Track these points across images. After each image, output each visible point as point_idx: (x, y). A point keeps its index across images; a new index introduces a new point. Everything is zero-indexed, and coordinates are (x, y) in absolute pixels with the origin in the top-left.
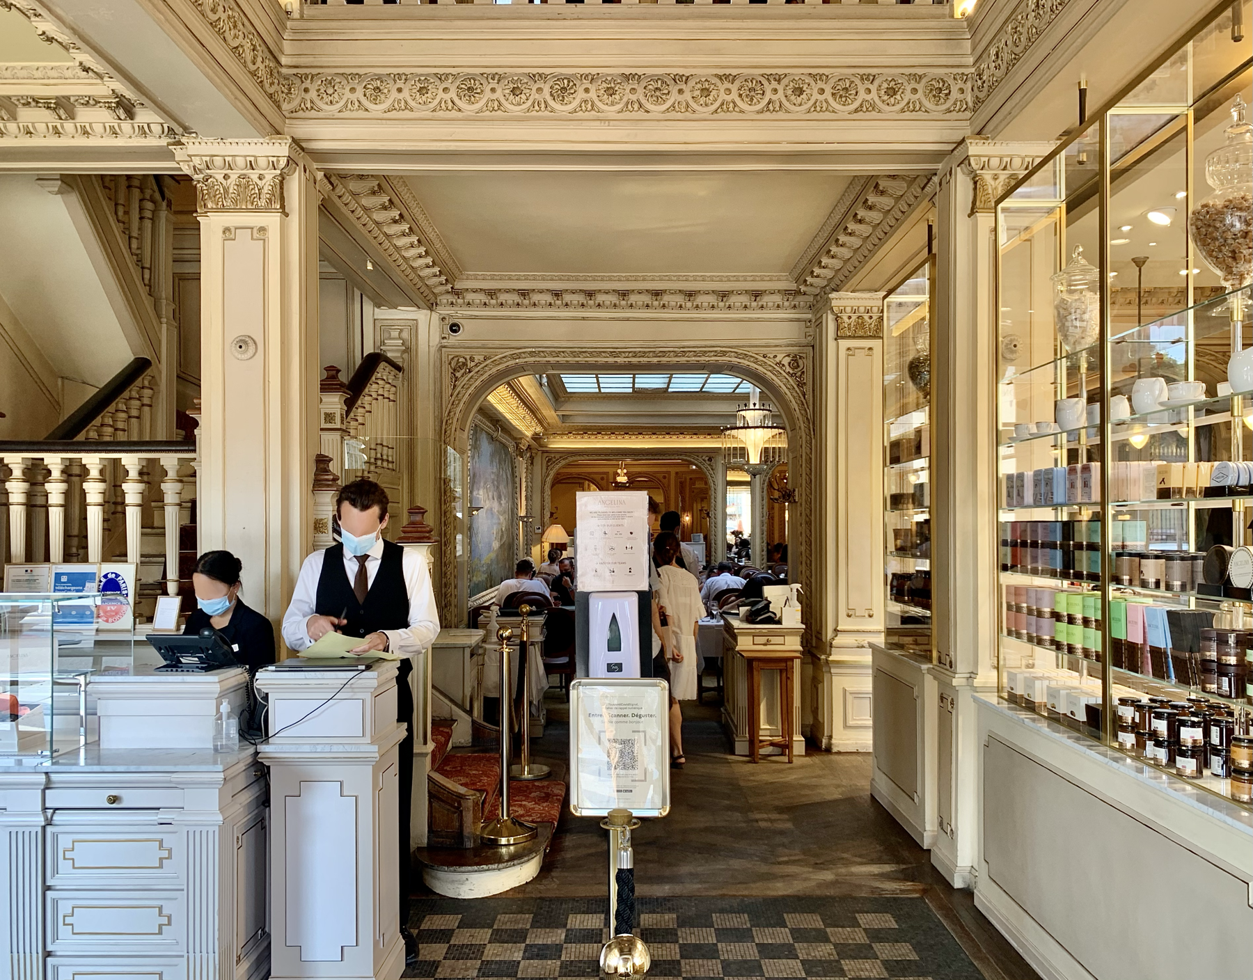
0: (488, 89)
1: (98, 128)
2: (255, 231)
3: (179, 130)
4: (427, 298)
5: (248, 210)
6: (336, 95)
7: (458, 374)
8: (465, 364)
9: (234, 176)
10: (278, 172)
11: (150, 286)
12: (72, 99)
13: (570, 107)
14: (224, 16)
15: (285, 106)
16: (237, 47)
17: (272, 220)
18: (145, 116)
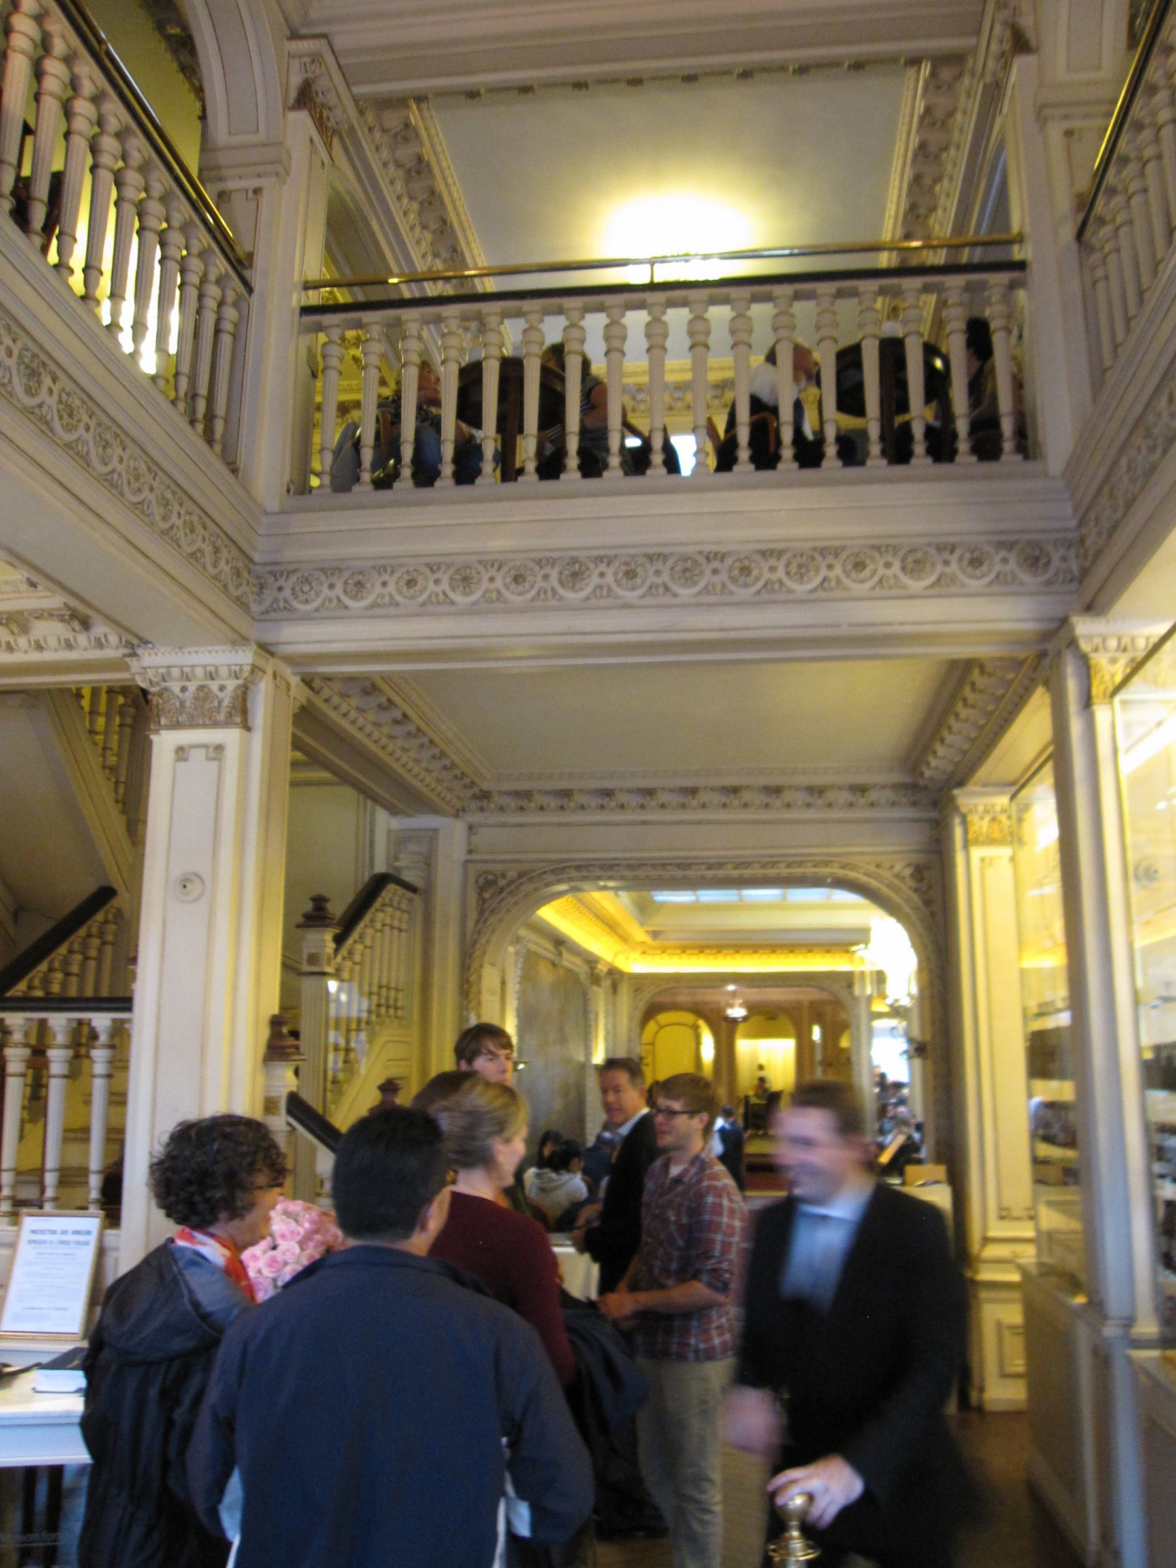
0: (486, 577)
1: (53, 642)
2: (211, 749)
3: (135, 641)
4: (451, 804)
5: (205, 726)
6: (313, 593)
7: (487, 895)
8: (494, 882)
9: (192, 687)
10: (241, 682)
11: (124, 803)
12: (26, 614)
13: (582, 595)
14: (179, 523)
15: (255, 608)
16: (195, 553)
17: (230, 737)
18: (100, 629)
